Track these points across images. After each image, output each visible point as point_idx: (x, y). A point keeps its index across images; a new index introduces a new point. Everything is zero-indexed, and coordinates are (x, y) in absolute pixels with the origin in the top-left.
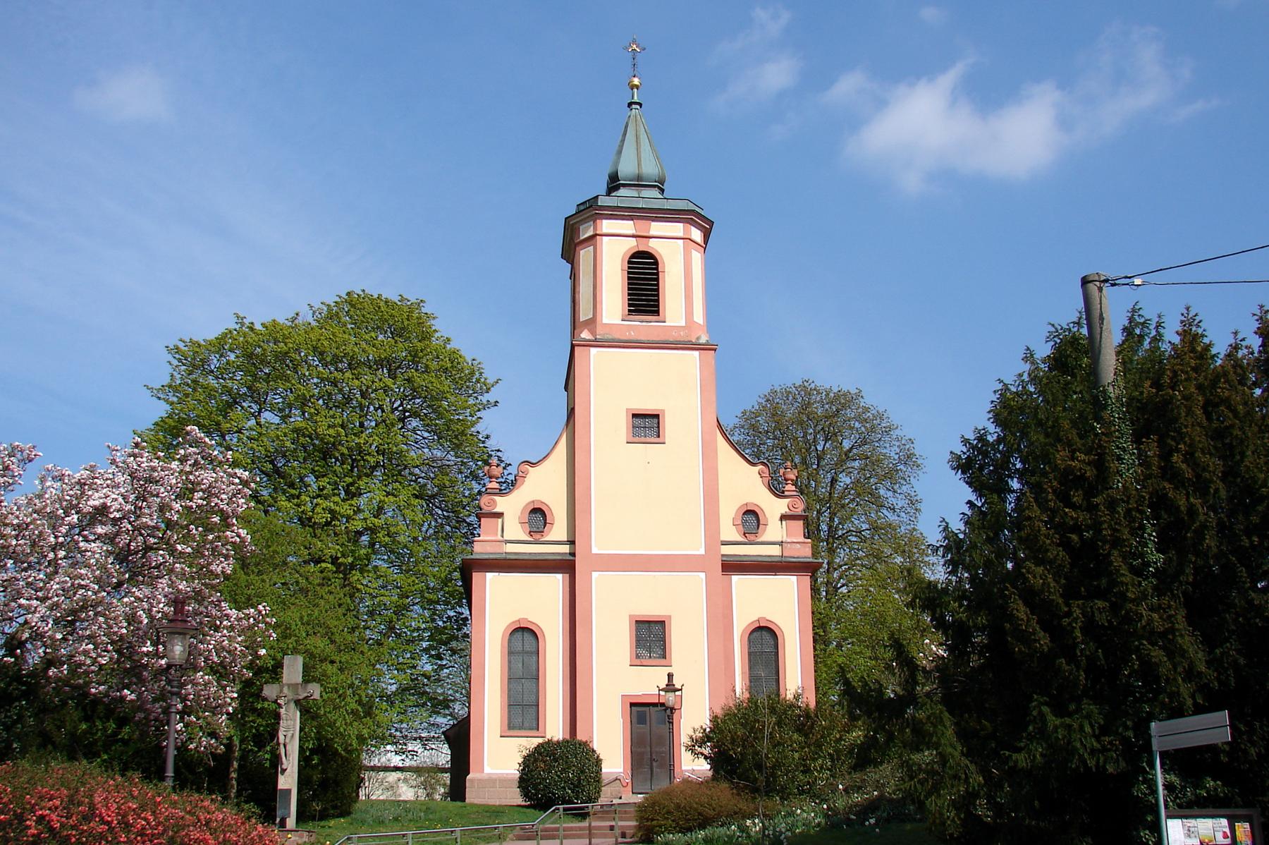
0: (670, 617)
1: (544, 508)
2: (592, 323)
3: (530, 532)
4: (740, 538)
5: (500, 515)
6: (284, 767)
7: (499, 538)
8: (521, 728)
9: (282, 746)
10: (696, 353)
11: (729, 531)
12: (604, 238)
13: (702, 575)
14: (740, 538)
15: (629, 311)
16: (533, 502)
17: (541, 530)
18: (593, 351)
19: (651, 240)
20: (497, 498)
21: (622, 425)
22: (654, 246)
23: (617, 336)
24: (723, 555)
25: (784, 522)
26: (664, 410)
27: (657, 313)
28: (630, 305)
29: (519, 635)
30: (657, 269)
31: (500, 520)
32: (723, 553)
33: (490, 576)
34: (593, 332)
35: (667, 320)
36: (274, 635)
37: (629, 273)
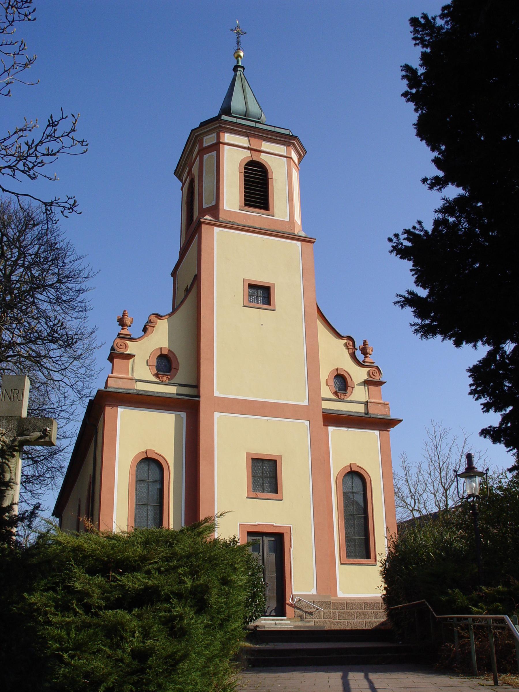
4: (333, 397)
5: (130, 356)
7: (130, 376)
10: (299, 243)
11: (326, 392)
12: (225, 146)
19: (262, 154)
22: (264, 158)
24: (323, 409)
32: (323, 407)
33: (121, 411)
36: (137, 586)
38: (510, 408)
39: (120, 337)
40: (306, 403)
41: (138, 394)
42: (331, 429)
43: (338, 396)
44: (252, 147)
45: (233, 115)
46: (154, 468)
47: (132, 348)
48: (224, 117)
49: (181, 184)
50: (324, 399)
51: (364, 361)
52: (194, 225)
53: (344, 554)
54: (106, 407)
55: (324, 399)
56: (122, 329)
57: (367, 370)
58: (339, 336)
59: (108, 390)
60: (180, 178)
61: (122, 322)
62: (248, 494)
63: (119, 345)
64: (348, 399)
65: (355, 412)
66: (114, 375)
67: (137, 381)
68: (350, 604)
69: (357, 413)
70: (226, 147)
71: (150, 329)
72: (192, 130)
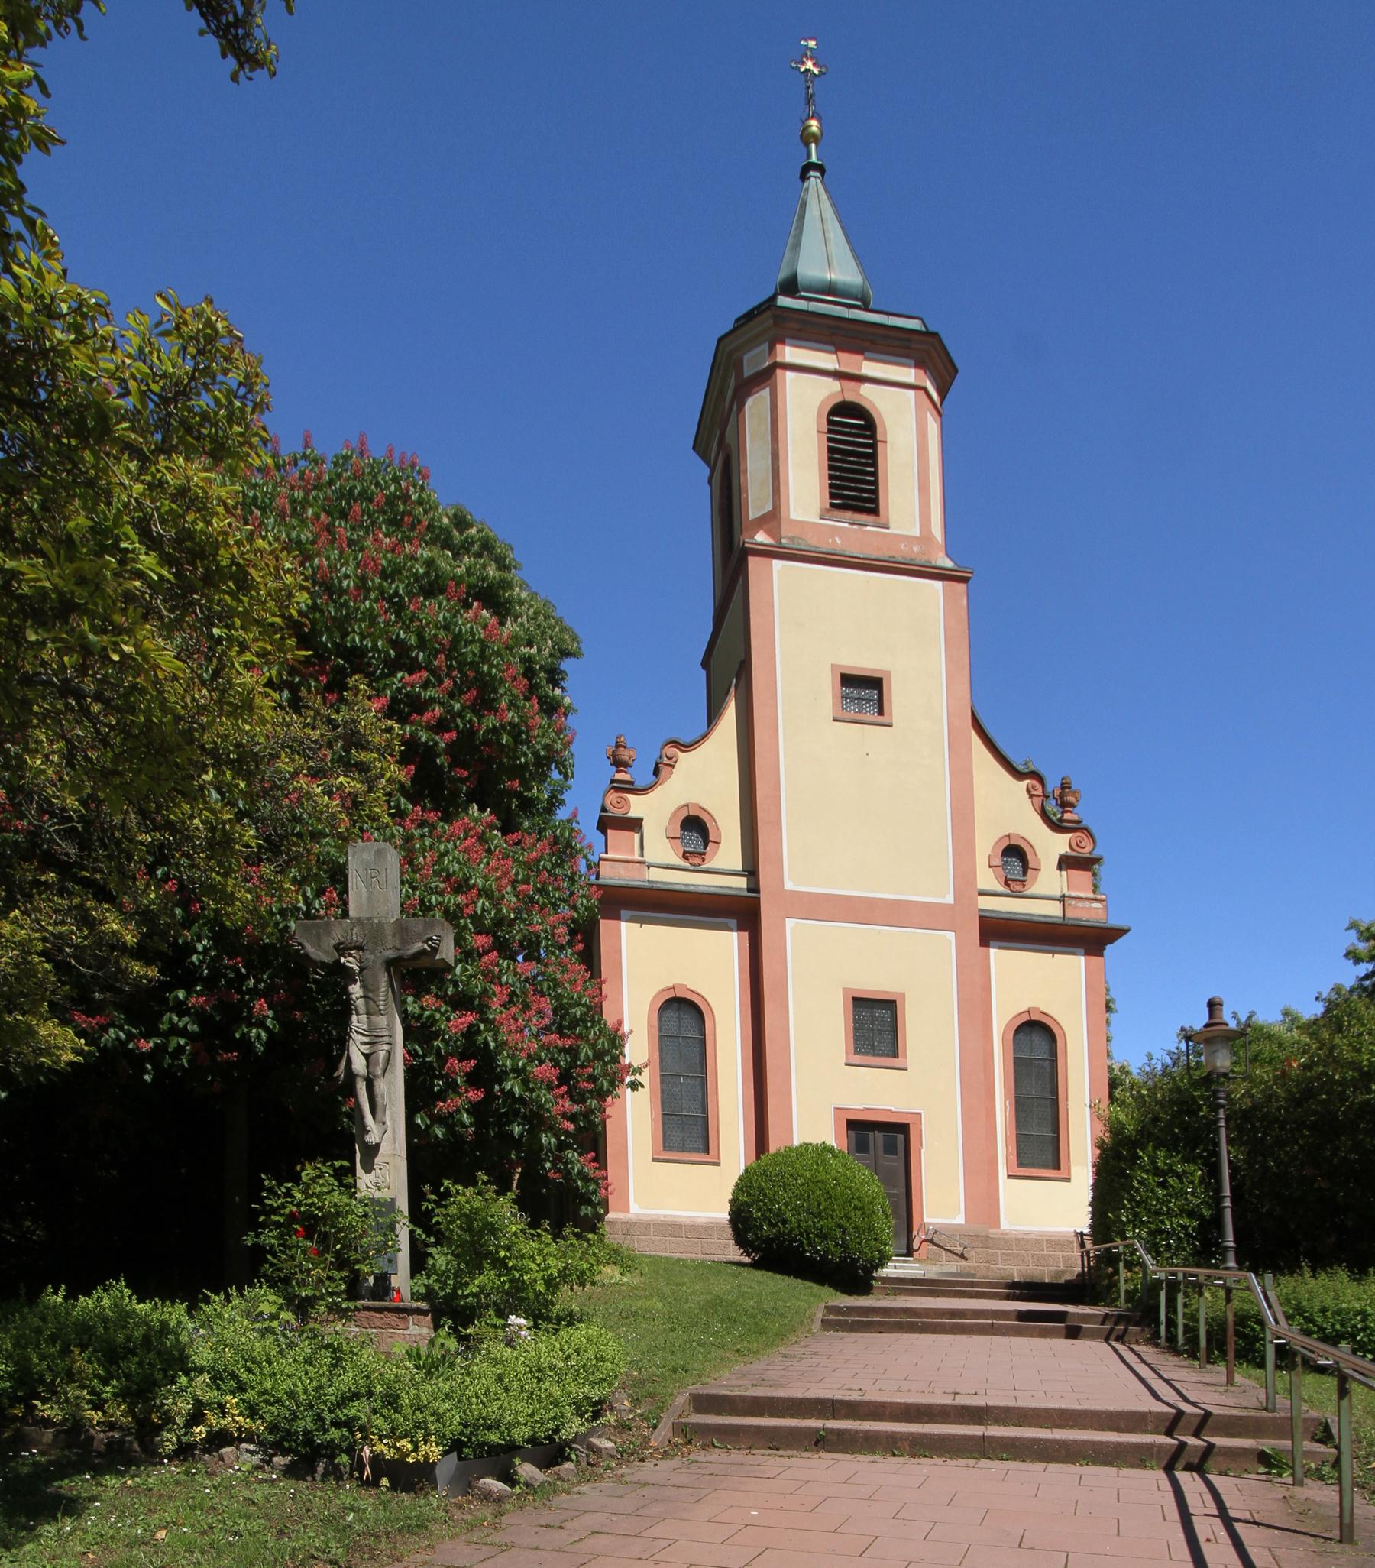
0: (903, 995)
1: (705, 817)
2: (772, 518)
3: (685, 852)
4: (1001, 889)
6: (372, 1138)
7: (637, 857)
8: (683, 1149)
9: (361, 1087)
10: (938, 585)
11: (988, 879)
13: (951, 936)
14: (1001, 889)
15: (832, 505)
16: (687, 805)
17: (701, 850)
18: (777, 564)
20: (630, 796)
21: (827, 689)
22: (869, 395)
23: (814, 542)
24: (980, 910)
25: (1064, 873)
26: (888, 673)
27: (874, 511)
28: (832, 496)
29: (672, 1014)
30: (873, 436)
31: (637, 836)
34: (774, 533)
35: (891, 525)
37: (829, 440)
38: (22, 1285)
39: (613, 788)
40: (949, 899)
41: (651, 889)
43: (1008, 886)
45: (803, 294)
46: (687, 1018)
47: (637, 805)
48: (784, 301)
49: (707, 471)
50: (982, 893)
51: (1061, 820)
52: (736, 555)
53: (1013, 1157)
55: (982, 893)
56: (618, 772)
57: (1068, 836)
58: (1017, 774)
60: (705, 457)
61: (618, 763)
62: (847, 1058)
64: (1028, 892)
65: (1039, 916)
66: (609, 856)
68: (1023, 1241)
70: (790, 375)
71: (664, 770)
72: (720, 340)
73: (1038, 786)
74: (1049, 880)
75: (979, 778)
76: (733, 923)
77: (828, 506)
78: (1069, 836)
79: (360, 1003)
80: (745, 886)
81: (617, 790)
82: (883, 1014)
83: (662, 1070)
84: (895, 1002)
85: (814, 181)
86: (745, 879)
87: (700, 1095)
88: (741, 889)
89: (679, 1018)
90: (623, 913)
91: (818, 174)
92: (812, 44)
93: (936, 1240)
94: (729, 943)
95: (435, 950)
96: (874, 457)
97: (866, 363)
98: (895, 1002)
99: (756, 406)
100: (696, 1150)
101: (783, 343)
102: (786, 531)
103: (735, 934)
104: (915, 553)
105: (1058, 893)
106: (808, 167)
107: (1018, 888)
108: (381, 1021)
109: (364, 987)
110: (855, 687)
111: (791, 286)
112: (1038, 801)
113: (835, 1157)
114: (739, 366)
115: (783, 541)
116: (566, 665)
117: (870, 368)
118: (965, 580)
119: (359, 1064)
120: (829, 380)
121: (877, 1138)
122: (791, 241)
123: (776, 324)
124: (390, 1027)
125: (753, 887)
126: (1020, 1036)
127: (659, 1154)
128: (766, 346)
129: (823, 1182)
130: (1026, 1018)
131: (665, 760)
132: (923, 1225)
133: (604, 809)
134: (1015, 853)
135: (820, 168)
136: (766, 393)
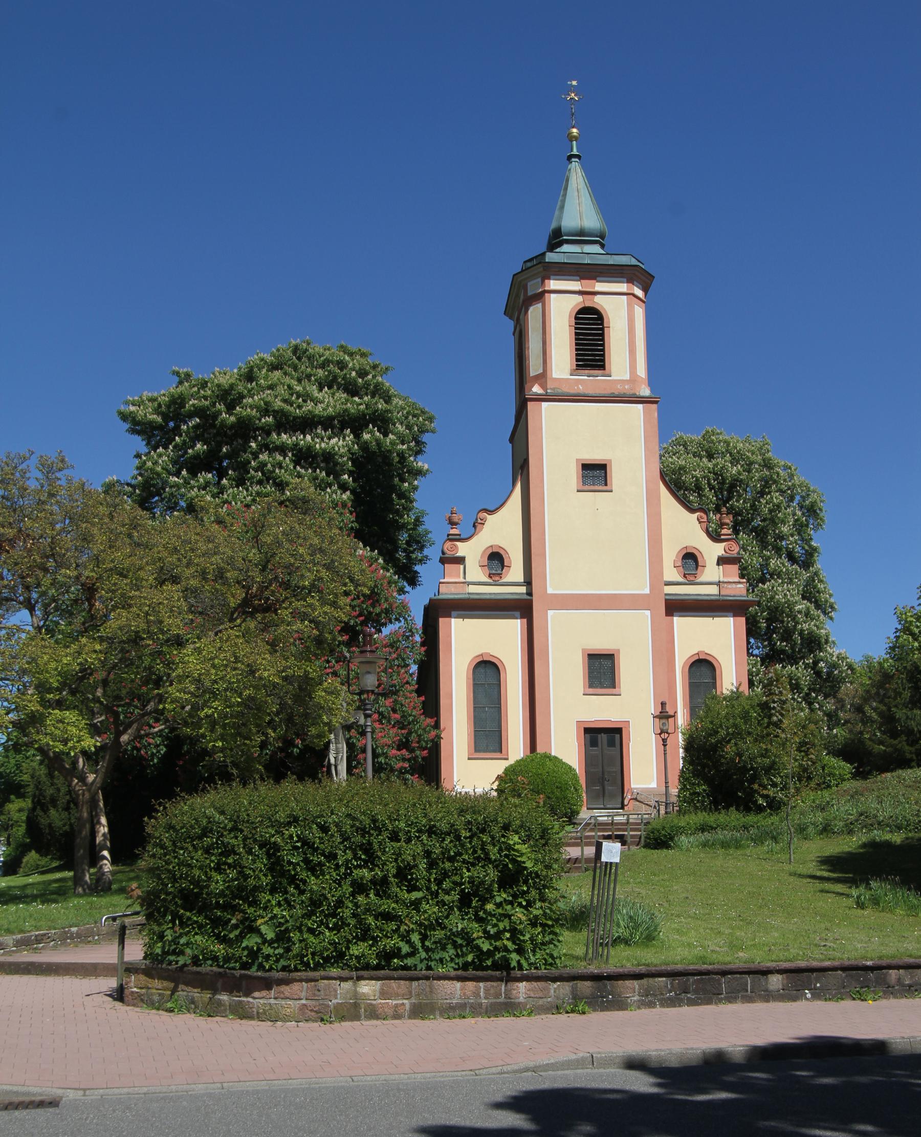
0: (618, 651)
1: (502, 552)
2: (542, 378)
3: (490, 574)
4: (681, 579)
7: (462, 580)
9: (333, 768)
11: (671, 573)
13: (648, 613)
14: (681, 579)
15: (577, 365)
16: (492, 546)
18: (545, 405)
20: (458, 543)
21: (573, 474)
22: (600, 302)
23: (566, 389)
24: (666, 595)
25: (721, 567)
26: (610, 461)
27: (602, 367)
28: (577, 360)
30: (602, 324)
31: (462, 567)
34: (543, 386)
37: (576, 329)
40: (647, 591)
42: (677, 620)
43: (686, 577)
44: (584, 289)
47: (462, 549)
54: (441, 620)
56: (452, 528)
59: (441, 597)
63: (450, 549)
64: (698, 580)
66: (445, 580)
67: (469, 584)
69: (708, 595)
70: (553, 296)
71: (479, 526)
72: (514, 275)
73: (704, 516)
74: (711, 572)
75: (665, 515)
76: (518, 614)
77: (575, 368)
78: (724, 544)
79: (333, 740)
80: (525, 592)
81: (451, 540)
82: (606, 663)
83: (474, 704)
84: (613, 655)
85: (575, 165)
86: (525, 588)
87: (497, 718)
88: (523, 594)
89: (486, 672)
90: (453, 613)
91: (577, 160)
92: (574, 83)
93: (638, 798)
94: (514, 627)
95: (358, 722)
96: (602, 335)
97: (597, 284)
98: (613, 655)
99: (534, 311)
100: (494, 751)
101: (549, 279)
102: (550, 385)
103: (519, 620)
104: (627, 389)
105: (716, 579)
106: (570, 157)
107: (692, 578)
108: (340, 746)
109: (335, 735)
110: (590, 470)
111: (557, 239)
112: (704, 525)
113: (550, 760)
114: (525, 288)
115: (549, 391)
116: (425, 438)
117: (599, 287)
118: (656, 402)
119: (332, 761)
120: (576, 296)
121: (603, 737)
122: (559, 203)
123: (544, 270)
124: (343, 747)
125: (529, 592)
126: (694, 668)
127: (472, 755)
128: (539, 280)
129: (541, 774)
130: (696, 658)
131: (479, 521)
132: (630, 789)
133: (443, 553)
134: (690, 559)
135: (578, 157)
136: (540, 305)
